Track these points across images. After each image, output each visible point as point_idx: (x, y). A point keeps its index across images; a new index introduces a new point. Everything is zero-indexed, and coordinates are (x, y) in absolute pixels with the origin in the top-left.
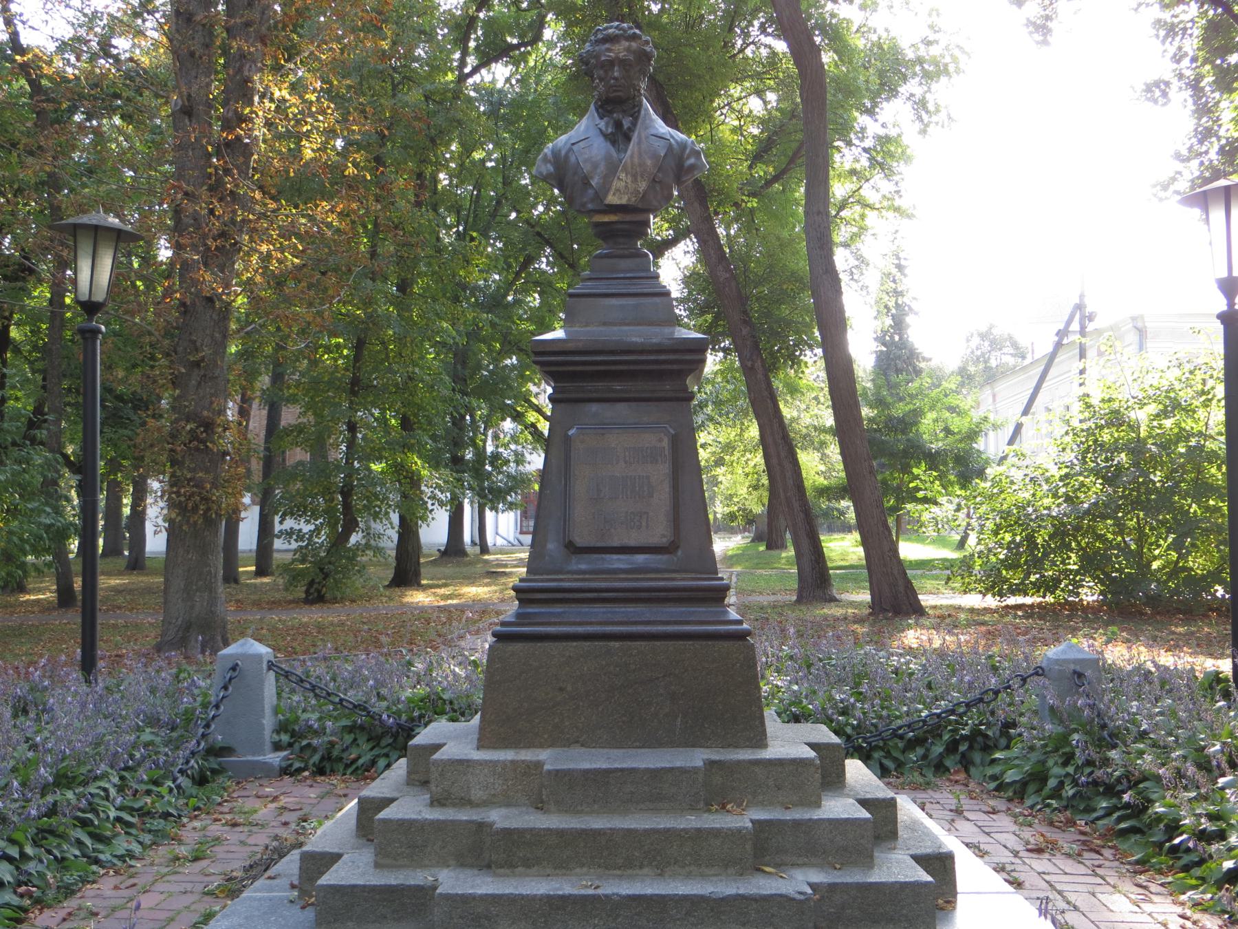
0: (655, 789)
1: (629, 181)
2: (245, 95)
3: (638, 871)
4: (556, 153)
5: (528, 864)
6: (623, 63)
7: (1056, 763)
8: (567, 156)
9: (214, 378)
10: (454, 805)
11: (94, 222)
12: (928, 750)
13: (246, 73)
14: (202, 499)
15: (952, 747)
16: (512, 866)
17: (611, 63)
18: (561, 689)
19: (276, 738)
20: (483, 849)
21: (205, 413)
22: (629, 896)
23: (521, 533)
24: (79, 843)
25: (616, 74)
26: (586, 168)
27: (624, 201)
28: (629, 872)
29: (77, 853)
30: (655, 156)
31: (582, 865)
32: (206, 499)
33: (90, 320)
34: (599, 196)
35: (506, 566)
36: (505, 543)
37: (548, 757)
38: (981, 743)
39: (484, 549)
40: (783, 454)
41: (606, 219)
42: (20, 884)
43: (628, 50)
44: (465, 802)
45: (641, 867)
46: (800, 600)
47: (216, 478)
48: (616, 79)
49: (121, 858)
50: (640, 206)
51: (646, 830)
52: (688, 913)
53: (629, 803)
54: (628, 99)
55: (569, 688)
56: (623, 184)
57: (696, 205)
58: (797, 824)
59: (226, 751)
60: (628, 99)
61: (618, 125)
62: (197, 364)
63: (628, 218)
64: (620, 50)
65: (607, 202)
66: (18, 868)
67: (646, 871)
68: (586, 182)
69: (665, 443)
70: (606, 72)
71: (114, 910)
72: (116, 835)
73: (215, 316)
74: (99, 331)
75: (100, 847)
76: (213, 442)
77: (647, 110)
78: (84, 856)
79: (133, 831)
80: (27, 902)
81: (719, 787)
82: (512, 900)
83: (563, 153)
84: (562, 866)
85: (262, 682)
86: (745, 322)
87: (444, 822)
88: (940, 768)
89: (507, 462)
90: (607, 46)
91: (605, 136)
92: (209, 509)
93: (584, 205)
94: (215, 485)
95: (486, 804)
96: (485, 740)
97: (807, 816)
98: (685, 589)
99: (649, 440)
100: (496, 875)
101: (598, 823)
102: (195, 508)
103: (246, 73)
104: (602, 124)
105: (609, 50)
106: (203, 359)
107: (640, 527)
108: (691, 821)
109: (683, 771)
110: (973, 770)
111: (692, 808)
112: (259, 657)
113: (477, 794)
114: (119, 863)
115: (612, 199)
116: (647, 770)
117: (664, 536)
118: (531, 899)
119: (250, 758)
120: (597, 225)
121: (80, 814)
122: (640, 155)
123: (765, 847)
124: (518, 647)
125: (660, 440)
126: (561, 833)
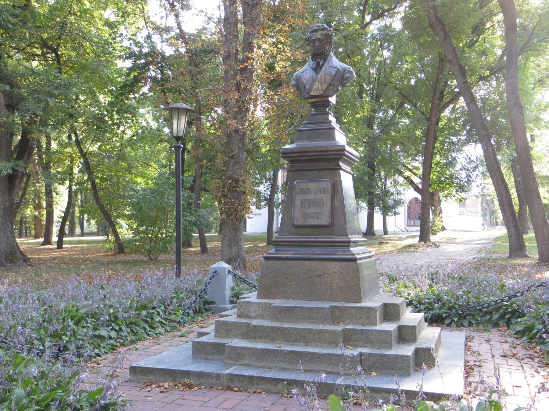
0: (311, 315)
2: (250, 49)
3: (298, 343)
4: (297, 76)
5: (261, 338)
6: (320, 40)
7: (539, 324)
9: (239, 162)
10: (245, 318)
11: (177, 107)
12: (492, 316)
13: (250, 40)
14: (234, 210)
15: (502, 317)
16: (255, 339)
17: (315, 40)
18: (287, 278)
19: (232, 299)
20: (252, 332)
21: (235, 176)
22: (289, 351)
23: (408, 226)
24: (144, 328)
25: (317, 44)
26: (305, 81)
27: (317, 93)
28: (296, 343)
29: (143, 331)
30: (330, 75)
31: (280, 340)
32: (235, 210)
33: (178, 143)
34: (308, 93)
35: (391, 240)
36: (400, 230)
37: (277, 302)
38: (517, 313)
39: (386, 232)
40: (502, 189)
41: (313, 100)
42: (118, 338)
43: (321, 34)
44: (249, 317)
45: (300, 342)
46: (510, 256)
47: (240, 201)
49: (156, 334)
51: (302, 329)
52: (310, 359)
53: (300, 319)
55: (289, 278)
57: (460, 76)
58: (362, 331)
59: (212, 303)
61: (318, 63)
62: (232, 157)
63: (320, 100)
64: (319, 35)
66: (118, 333)
67: (301, 343)
69: (330, 186)
71: (144, 349)
72: (158, 327)
73: (239, 138)
74: (181, 147)
75: (151, 330)
76: (238, 188)
78: (146, 333)
79: (165, 326)
80: (119, 344)
81: (335, 315)
82: (250, 349)
84: (272, 340)
85: (225, 278)
86: (483, 129)
87: (237, 322)
88: (496, 325)
89: (392, 194)
91: (313, 69)
92: (237, 214)
93: (304, 96)
94: (239, 205)
95: (255, 318)
96: (259, 297)
97: (370, 329)
98: (305, 242)
99: (323, 185)
100: (250, 341)
101: (286, 325)
102: (232, 214)
103: (250, 40)
105: (314, 35)
106: (235, 155)
107: (318, 218)
108: (322, 327)
109: (320, 309)
110: (511, 326)
111: (323, 323)
112: (224, 269)
113: (253, 314)
114: (155, 336)
115: (313, 93)
116: (307, 308)
117: (327, 221)
118: (257, 349)
119: (220, 306)
121: (145, 318)
123: (348, 338)
124: (272, 262)
125: (328, 185)
126: (272, 328)
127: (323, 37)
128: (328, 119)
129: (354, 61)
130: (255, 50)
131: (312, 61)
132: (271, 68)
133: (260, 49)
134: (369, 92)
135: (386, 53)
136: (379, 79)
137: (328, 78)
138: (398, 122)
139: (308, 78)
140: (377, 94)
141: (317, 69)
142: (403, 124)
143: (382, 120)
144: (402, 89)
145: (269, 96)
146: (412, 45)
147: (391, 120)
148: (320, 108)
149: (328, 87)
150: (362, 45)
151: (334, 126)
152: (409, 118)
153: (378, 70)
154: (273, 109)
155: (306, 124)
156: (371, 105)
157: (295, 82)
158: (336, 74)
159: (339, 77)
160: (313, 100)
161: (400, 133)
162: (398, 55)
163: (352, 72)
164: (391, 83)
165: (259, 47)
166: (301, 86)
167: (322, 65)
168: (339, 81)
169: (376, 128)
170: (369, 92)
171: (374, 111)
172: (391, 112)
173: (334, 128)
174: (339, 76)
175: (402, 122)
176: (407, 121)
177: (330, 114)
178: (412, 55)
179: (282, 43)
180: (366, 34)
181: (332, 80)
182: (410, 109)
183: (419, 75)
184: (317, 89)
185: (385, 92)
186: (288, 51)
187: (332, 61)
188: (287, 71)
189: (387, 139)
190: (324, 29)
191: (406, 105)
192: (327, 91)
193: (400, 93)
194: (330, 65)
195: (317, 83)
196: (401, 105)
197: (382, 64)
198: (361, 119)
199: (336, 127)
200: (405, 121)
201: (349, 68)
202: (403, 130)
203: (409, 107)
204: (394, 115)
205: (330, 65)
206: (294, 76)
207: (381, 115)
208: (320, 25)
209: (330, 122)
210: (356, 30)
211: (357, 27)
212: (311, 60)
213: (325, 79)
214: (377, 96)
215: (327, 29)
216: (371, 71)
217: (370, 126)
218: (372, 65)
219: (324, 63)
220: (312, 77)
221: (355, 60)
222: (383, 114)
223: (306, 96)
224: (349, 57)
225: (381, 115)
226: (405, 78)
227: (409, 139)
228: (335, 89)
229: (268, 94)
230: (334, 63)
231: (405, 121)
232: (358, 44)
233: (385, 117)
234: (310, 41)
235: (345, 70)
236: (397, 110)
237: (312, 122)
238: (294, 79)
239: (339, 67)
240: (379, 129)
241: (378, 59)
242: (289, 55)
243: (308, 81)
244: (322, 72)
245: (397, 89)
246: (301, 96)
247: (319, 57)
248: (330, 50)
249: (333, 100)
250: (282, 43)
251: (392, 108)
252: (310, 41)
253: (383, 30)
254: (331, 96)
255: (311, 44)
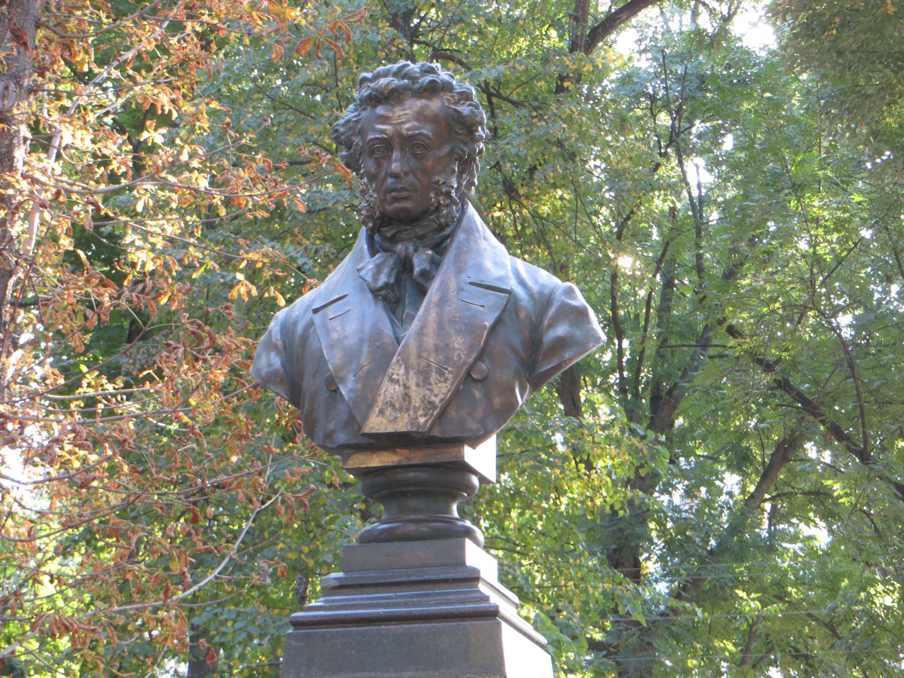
1: (412, 383)
4: (287, 329)
8: (305, 337)
17: (387, 144)
25: (395, 167)
26: (334, 359)
27: (402, 425)
30: (470, 327)
34: (353, 422)
41: (376, 461)
43: (420, 116)
48: (396, 176)
50: (436, 433)
54: (426, 213)
56: (399, 389)
60: (426, 213)
61: (405, 265)
63: (418, 457)
64: (405, 117)
65: (366, 430)
68: (332, 386)
70: (378, 163)
77: (472, 221)
83: (300, 328)
90: (380, 110)
93: (329, 436)
104: (739, 44)
105: (384, 119)
115: (376, 424)
120: (364, 473)
122: (440, 326)
127: (427, 130)
128: (460, 562)
129: (536, 215)
130: (20, 154)
131: (373, 252)
132: (99, 245)
133: (46, 149)
134: (614, 378)
135: (698, 174)
136: (665, 308)
137: (458, 343)
138: (772, 535)
139: (351, 341)
140: (655, 384)
141: (400, 292)
142: (797, 547)
143: (682, 525)
144: (794, 364)
145: (91, 402)
146: (836, 140)
147: (736, 528)
148: (414, 503)
149: (457, 393)
150: (583, 136)
151: (495, 599)
152: (829, 514)
153: (664, 262)
154: (113, 470)
155: (342, 587)
156: (634, 451)
157: (276, 361)
158: (498, 322)
159: (516, 341)
160: (376, 461)
161: (781, 597)
162: (767, 183)
163: (581, 313)
164: (732, 331)
165: (42, 141)
166: (311, 383)
167: (428, 276)
168: (514, 364)
169: (651, 567)
170: (614, 378)
171: (644, 481)
172: (731, 481)
173: (494, 613)
174: (514, 336)
175: (794, 539)
176: (820, 535)
177: (469, 533)
178: (840, 185)
179: (165, 120)
180: (600, 74)
181: (479, 358)
182: (833, 470)
183: (877, 290)
184: (398, 403)
185: (700, 379)
186: (195, 164)
187: (479, 253)
188: (191, 267)
189: (713, 631)
190: (434, 89)
191: (811, 450)
192: (452, 413)
193: (783, 385)
194: (470, 275)
195: (398, 371)
196: (787, 450)
197: (686, 227)
198: (574, 520)
199: (506, 610)
200: (805, 530)
201: (569, 292)
202: (799, 582)
203: (827, 457)
204: (753, 502)
205: (470, 275)
206: (274, 326)
207: (677, 498)
208: (414, 67)
209: (474, 578)
210: (546, 58)
211: (554, 39)
212: (362, 243)
213: (443, 348)
214: (655, 400)
215: (447, 87)
216: (626, 263)
217: (623, 557)
218: (625, 232)
219: (436, 264)
220: (376, 336)
221: (545, 210)
222: (689, 493)
223: (342, 438)
224: (510, 190)
225: (677, 498)
226: (805, 308)
227: (831, 627)
228: (497, 401)
229: (84, 390)
230: (488, 264)
231: (805, 530)
232: (559, 130)
233: (699, 513)
234: (361, 151)
235: (544, 300)
236: (767, 474)
237: (372, 576)
238: (270, 346)
239: (512, 284)
240: (669, 574)
241: (660, 203)
242: (203, 183)
243: (352, 356)
244: (426, 312)
245: (768, 367)
246: (311, 434)
247: (411, 233)
248: (463, 198)
249: (482, 458)
250: (165, 120)
251: (740, 461)
252: (361, 151)
253: (683, 57)
254: (474, 441)
255: (368, 164)
